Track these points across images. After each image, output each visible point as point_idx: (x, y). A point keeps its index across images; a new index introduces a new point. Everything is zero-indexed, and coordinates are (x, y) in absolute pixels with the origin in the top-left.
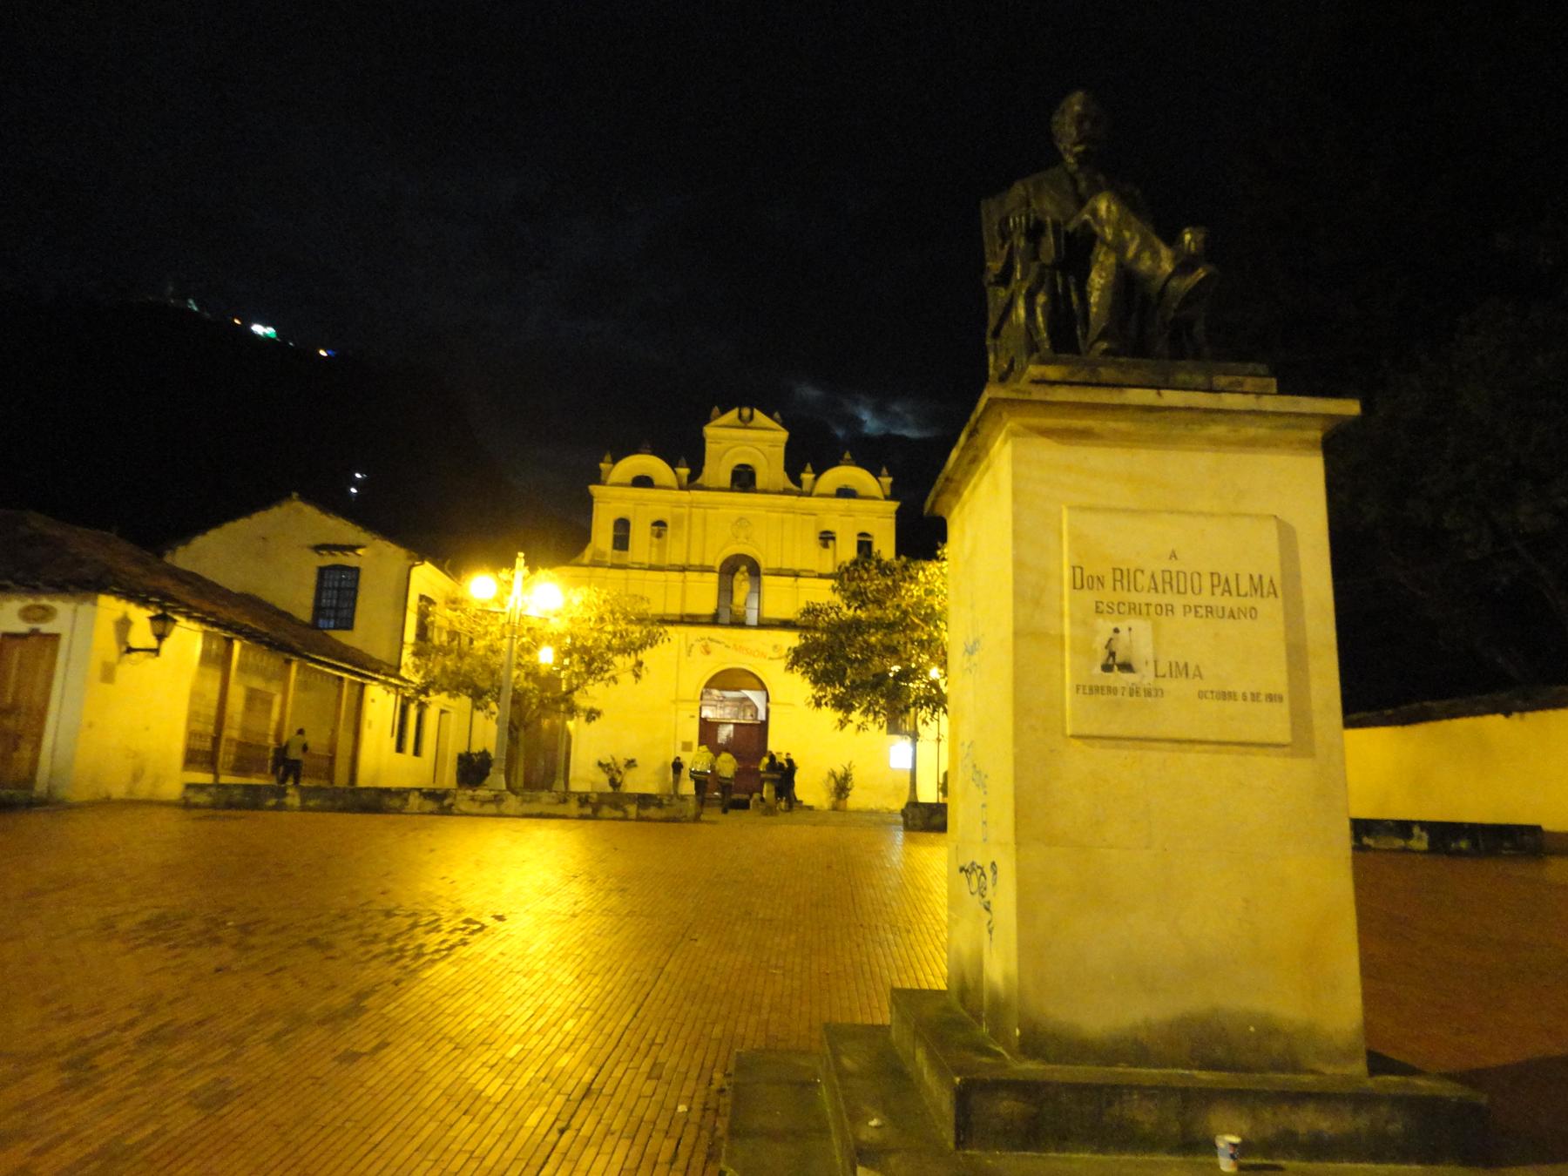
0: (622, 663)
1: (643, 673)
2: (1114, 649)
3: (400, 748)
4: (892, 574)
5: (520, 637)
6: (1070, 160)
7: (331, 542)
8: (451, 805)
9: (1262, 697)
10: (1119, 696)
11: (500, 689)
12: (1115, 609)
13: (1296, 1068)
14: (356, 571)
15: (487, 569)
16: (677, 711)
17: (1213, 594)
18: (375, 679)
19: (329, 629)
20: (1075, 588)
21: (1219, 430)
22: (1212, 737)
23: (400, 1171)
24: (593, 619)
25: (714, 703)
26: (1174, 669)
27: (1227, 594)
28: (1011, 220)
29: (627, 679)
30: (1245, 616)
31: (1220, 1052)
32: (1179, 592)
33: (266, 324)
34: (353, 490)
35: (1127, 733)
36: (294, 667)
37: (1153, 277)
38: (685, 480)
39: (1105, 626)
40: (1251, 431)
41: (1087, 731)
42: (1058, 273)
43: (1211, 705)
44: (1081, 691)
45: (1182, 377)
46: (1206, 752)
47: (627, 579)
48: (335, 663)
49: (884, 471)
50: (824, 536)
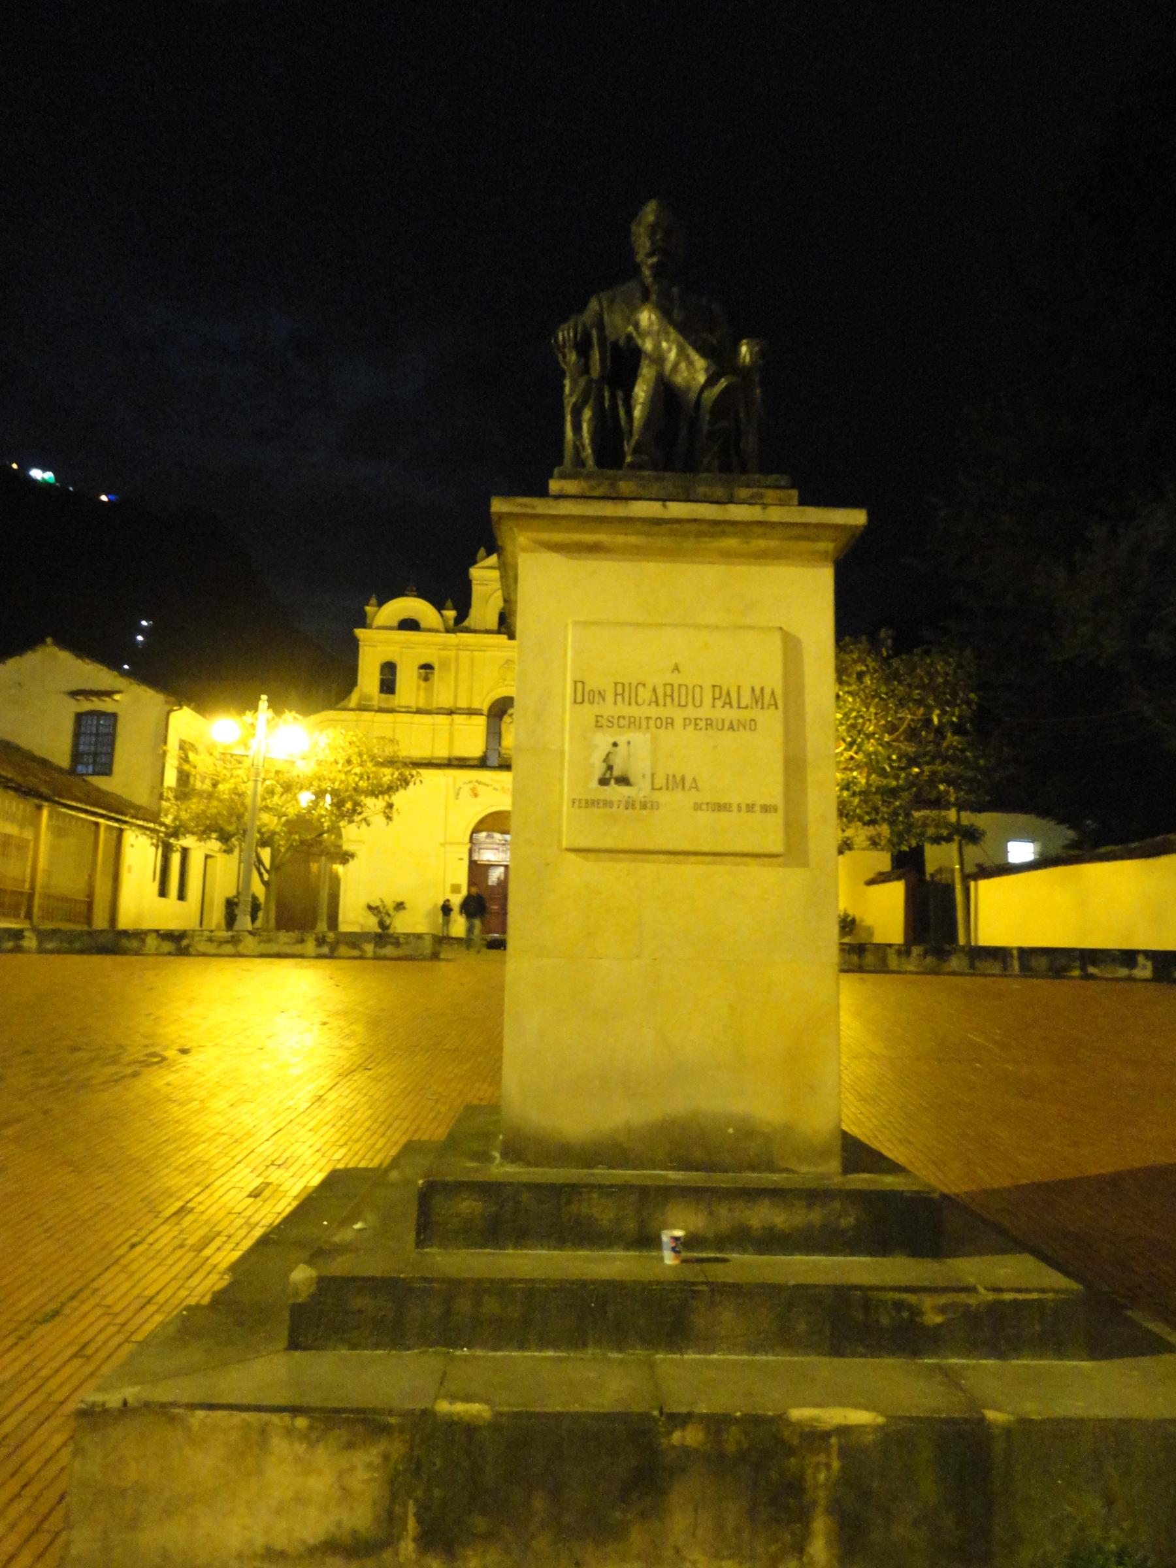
0: (373, 805)
1: (395, 815)
3: (163, 892)
5: (264, 780)
6: (647, 272)
7: (88, 688)
8: (188, 946)
9: (757, 808)
10: (615, 809)
11: (245, 831)
12: (615, 723)
14: (114, 716)
15: (233, 712)
16: (445, 853)
17: (714, 706)
18: (132, 824)
19: (87, 774)
21: (731, 543)
22: (706, 849)
24: (341, 761)
25: (495, 846)
27: (727, 706)
28: (560, 334)
29: (379, 820)
30: (745, 727)
31: (698, 1154)
32: (679, 705)
34: (140, 638)
35: (621, 846)
36: (45, 813)
37: (688, 389)
38: (452, 622)
39: (603, 742)
40: (762, 543)
41: (577, 845)
42: (606, 388)
43: (704, 816)
44: (577, 804)
45: (702, 490)
46: (703, 863)
47: (394, 723)
48: (88, 808)
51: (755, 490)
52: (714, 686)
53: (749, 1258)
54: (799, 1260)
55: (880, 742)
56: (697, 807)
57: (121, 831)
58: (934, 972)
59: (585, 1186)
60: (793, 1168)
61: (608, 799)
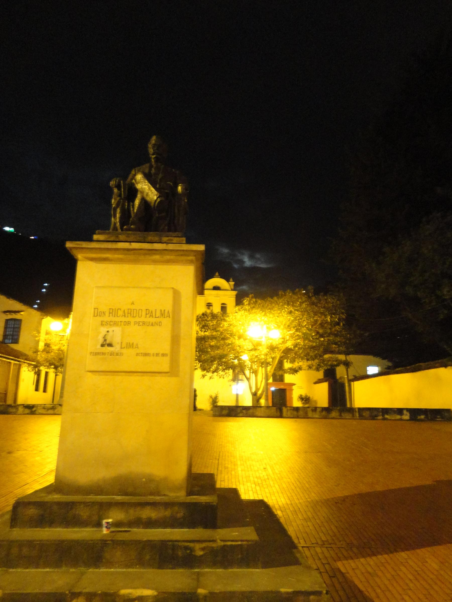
2: (106, 339)
3: (37, 389)
4: (217, 318)
6: (153, 160)
8: (35, 411)
9: (160, 355)
12: (109, 324)
13: (158, 494)
14: (20, 321)
17: (146, 317)
18: (25, 363)
20: (94, 316)
21: (157, 257)
22: (140, 370)
23: (326, 582)
26: (128, 345)
30: (157, 325)
31: (130, 490)
33: (10, 227)
35: (108, 370)
39: (103, 330)
40: (168, 257)
41: (90, 370)
43: (141, 358)
44: (92, 354)
45: (150, 238)
46: (138, 376)
48: (6, 356)
49: (231, 280)
50: (208, 305)
51: (170, 238)
52: (147, 310)
53: (141, 530)
54: (177, 531)
55: (308, 329)
56: (137, 354)
57: (20, 366)
58: (325, 418)
59: (79, 503)
60: (166, 493)
61: (104, 352)
